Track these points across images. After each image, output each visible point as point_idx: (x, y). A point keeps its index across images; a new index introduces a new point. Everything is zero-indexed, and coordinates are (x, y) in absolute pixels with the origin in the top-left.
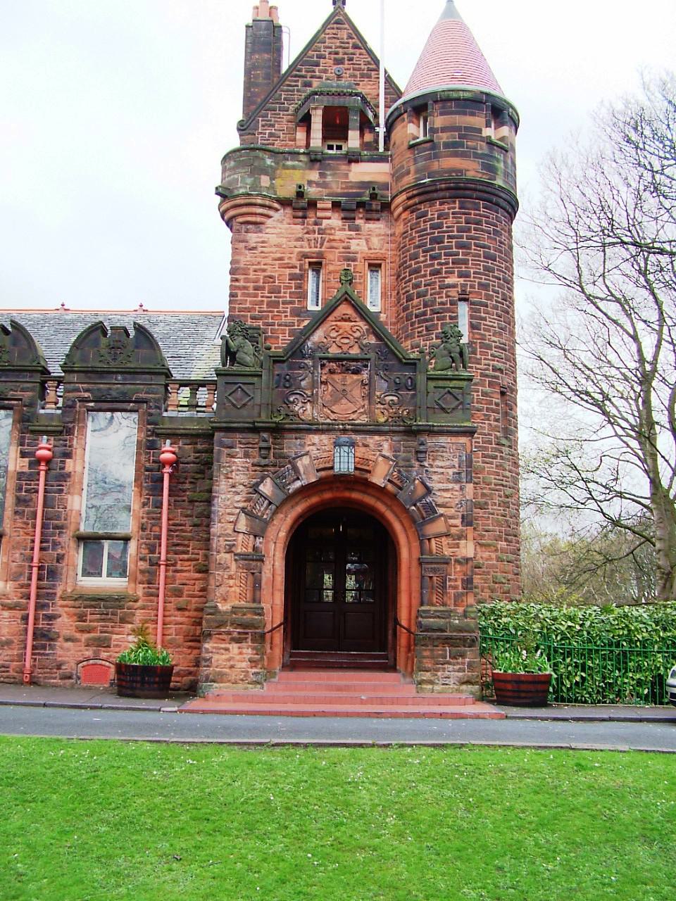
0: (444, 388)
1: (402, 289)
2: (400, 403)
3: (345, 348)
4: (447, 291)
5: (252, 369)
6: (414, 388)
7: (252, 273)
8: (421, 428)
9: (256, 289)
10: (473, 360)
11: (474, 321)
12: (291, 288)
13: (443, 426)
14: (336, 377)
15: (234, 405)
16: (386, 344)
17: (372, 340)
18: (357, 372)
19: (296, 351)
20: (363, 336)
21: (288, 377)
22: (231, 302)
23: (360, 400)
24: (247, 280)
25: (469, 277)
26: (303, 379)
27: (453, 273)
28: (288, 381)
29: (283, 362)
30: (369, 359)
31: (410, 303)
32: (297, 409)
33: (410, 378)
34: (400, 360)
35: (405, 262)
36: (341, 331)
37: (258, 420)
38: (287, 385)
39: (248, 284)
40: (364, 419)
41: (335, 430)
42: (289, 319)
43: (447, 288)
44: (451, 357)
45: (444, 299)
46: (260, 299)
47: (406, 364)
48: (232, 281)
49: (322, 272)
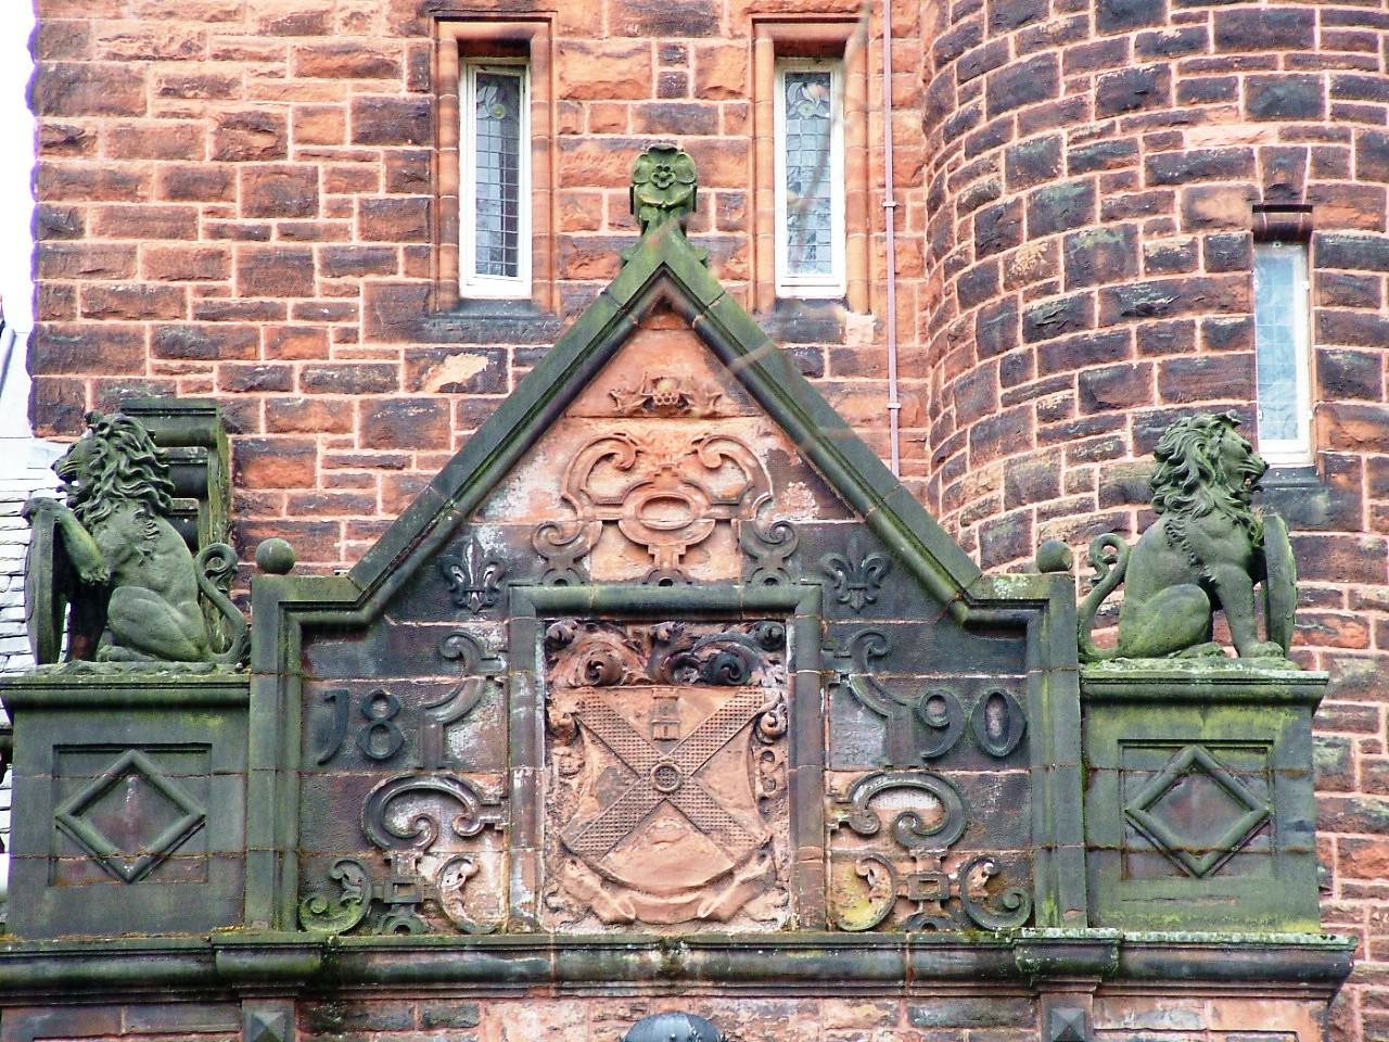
0: (1175, 745)
1: (956, 182)
2: (954, 829)
3: (667, 553)
4: (1194, 196)
5: (195, 672)
6: (1019, 751)
7: (156, 104)
8: (1061, 957)
9: (181, 188)
10: (1340, 559)
11: (1341, 353)
12: (369, 181)
13: (1172, 946)
14: (632, 704)
15: (99, 858)
16: (872, 526)
17: (802, 508)
18: (728, 675)
19: (423, 574)
20: (752, 488)
21: (381, 709)
22: (41, 261)
23: (749, 816)
24: (131, 144)
25: (1312, 108)
26: (460, 719)
27: (1225, 92)
28: (381, 728)
29: (356, 631)
30: (790, 609)
31: (999, 257)
32: (429, 868)
33: (996, 697)
34: (948, 614)
35: (970, 36)
36: (645, 469)
37: (230, 934)
38: (377, 753)
39: (136, 166)
40: (768, 916)
41: (620, 974)
42: (368, 351)
43: (1190, 175)
44: (1209, 586)
45: (1178, 240)
46: (203, 243)
47: (974, 627)
48: (46, 146)
49: (531, 91)
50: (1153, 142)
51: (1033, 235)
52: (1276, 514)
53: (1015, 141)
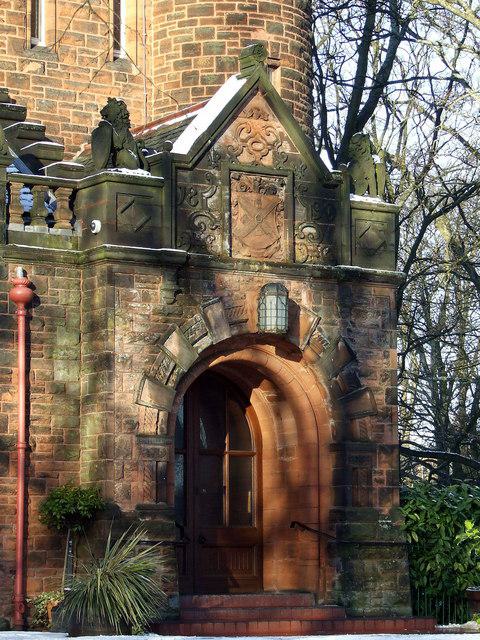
25: (281, 32)
27: (260, 23)
50: (243, 34)
51: (205, 54)
52: (332, 171)
53: (198, 26)
